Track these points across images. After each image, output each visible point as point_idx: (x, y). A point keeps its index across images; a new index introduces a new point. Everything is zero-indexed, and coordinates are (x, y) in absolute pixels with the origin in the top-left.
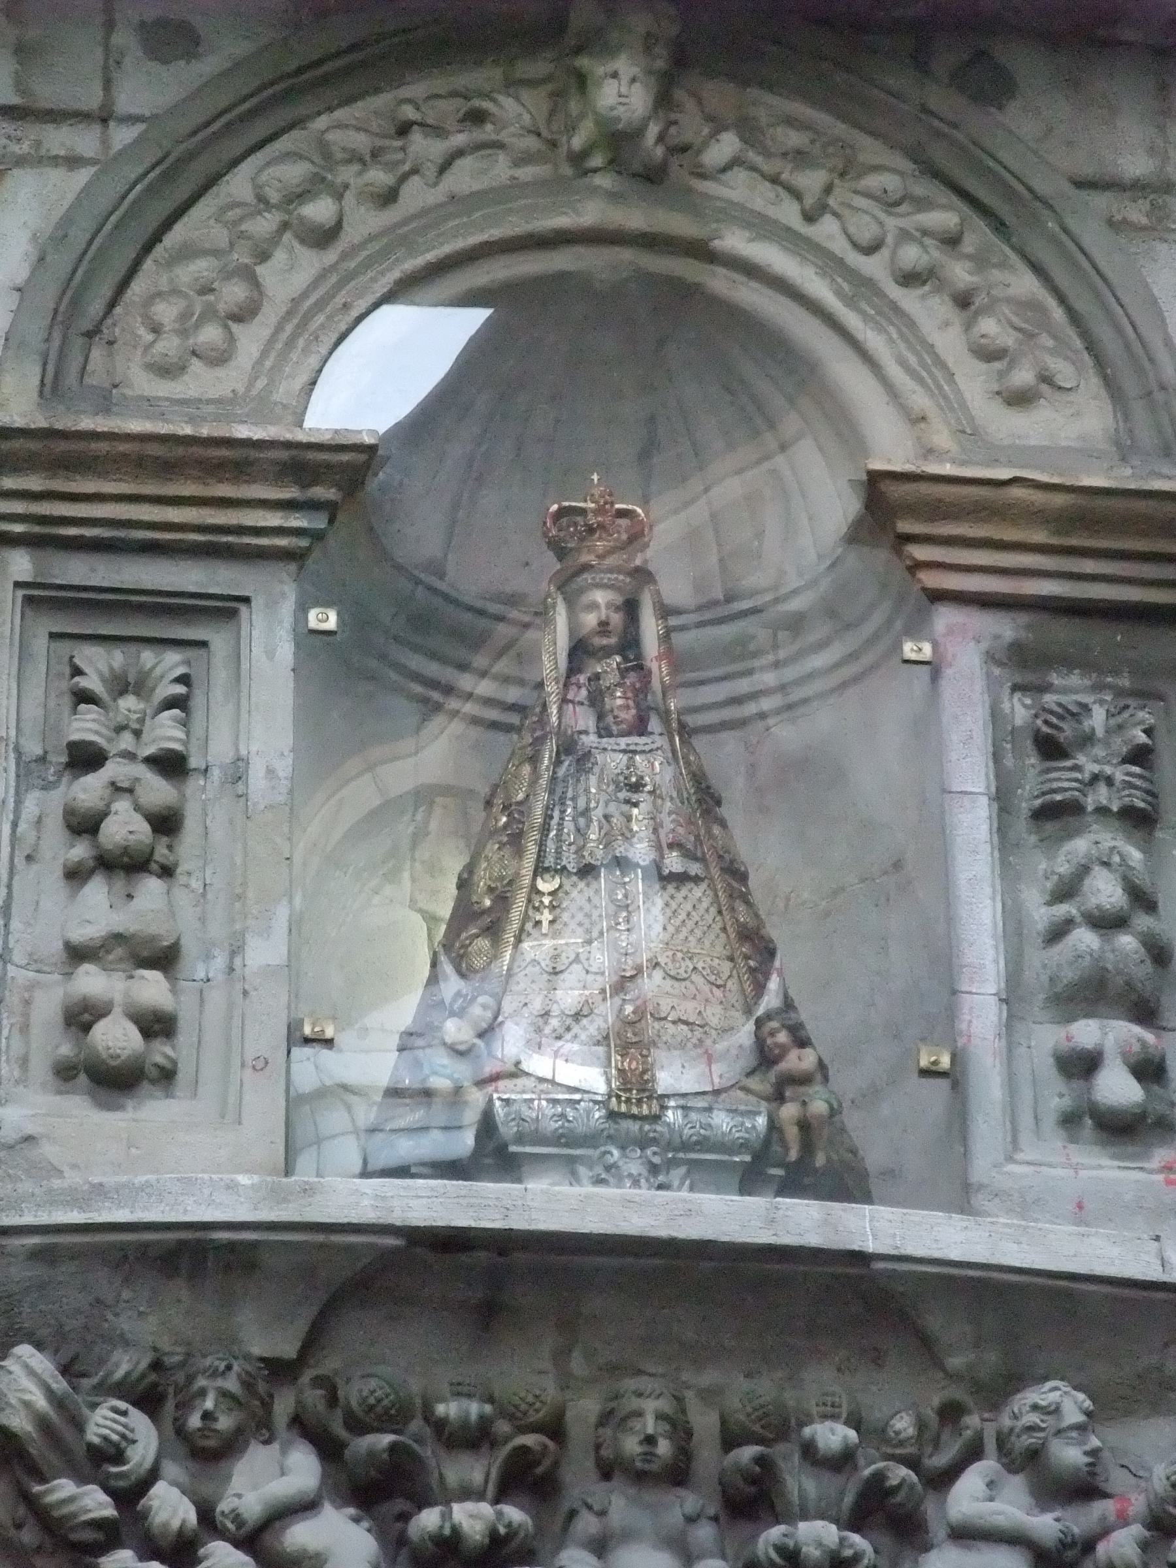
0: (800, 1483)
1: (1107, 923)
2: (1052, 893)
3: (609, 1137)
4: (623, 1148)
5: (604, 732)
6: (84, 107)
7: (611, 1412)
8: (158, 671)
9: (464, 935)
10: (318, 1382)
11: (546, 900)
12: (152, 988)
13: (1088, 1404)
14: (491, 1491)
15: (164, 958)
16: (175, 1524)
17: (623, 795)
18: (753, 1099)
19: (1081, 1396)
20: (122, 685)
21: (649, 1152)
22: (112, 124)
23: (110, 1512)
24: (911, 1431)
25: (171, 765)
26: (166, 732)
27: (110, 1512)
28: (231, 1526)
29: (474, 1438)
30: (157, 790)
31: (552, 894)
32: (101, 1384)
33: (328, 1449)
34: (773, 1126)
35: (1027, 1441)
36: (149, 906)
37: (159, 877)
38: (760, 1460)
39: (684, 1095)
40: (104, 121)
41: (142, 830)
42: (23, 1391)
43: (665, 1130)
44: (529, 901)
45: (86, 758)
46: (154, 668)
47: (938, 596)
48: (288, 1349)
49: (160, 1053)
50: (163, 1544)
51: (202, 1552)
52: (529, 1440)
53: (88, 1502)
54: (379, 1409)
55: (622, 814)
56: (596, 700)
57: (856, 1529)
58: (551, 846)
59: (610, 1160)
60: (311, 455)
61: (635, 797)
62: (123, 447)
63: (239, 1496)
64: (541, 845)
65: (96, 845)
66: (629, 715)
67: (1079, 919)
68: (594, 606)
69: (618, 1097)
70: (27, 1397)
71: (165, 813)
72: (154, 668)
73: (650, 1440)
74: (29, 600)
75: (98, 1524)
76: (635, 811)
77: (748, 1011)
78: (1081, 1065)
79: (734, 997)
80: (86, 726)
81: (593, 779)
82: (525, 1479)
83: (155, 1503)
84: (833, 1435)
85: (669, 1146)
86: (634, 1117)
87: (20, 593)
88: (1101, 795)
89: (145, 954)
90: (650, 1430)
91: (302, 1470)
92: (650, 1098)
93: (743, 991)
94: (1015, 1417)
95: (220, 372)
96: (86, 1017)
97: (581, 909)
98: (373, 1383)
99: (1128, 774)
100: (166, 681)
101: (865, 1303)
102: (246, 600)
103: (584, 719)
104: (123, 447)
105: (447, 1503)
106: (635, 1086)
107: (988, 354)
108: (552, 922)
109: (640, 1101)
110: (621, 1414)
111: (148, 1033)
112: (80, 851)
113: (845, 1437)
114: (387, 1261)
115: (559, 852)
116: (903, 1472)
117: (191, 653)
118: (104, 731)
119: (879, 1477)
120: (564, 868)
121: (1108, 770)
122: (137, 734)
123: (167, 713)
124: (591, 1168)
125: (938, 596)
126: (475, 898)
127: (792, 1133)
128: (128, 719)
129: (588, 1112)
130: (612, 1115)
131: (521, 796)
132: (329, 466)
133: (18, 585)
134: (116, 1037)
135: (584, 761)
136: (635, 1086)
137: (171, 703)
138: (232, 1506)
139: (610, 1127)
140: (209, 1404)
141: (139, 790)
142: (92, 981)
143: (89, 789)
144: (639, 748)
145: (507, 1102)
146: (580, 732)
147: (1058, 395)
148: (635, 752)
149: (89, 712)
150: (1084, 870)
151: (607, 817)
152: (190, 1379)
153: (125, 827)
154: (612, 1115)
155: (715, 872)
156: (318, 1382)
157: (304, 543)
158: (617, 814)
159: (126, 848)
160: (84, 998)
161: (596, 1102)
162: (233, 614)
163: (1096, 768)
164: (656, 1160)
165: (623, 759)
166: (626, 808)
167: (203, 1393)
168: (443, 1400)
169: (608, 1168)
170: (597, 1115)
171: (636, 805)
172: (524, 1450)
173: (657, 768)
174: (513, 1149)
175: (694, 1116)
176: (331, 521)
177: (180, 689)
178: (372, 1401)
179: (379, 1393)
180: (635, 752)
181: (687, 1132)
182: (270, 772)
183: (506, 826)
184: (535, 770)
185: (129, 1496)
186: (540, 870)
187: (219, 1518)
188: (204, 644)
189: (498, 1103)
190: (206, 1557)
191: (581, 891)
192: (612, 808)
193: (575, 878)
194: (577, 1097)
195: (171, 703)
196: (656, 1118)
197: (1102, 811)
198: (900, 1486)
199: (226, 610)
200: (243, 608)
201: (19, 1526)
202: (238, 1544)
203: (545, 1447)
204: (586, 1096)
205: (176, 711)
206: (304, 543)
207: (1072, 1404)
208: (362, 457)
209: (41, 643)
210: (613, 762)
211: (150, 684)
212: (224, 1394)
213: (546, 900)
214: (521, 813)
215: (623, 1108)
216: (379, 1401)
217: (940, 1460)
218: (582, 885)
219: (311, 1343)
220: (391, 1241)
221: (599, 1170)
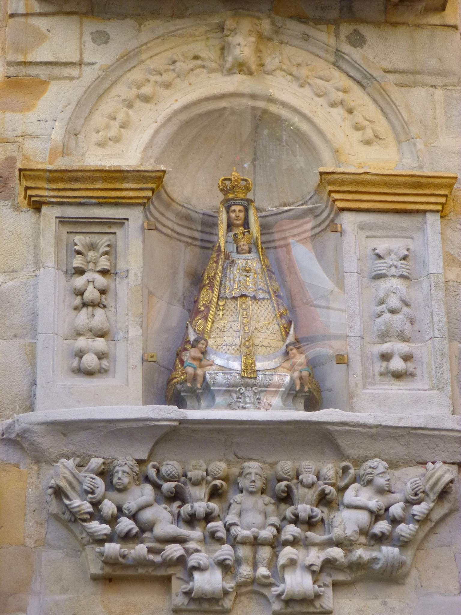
0: (299, 492)
1: (393, 311)
2: (378, 303)
3: (242, 384)
4: (246, 387)
5: (238, 252)
6: (74, 61)
7: (242, 472)
8: (100, 244)
9: (196, 319)
10: (154, 467)
11: (221, 308)
12: (100, 344)
13: (387, 465)
14: (207, 498)
15: (102, 334)
16: (110, 513)
17: (244, 273)
18: (285, 370)
19: (384, 463)
20: (92, 247)
21: (254, 389)
22: (83, 66)
23: (91, 510)
24: (334, 475)
25: (104, 272)
26: (104, 263)
27: (91, 510)
28: (127, 512)
29: (196, 483)
30: (101, 280)
31: (223, 305)
32: (88, 469)
33: (157, 487)
34: (291, 378)
35: (369, 477)
36: (99, 318)
37: (102, 308)
38: (288, 486)
39: (264, 370)
40: (80, 65)
41: (97, 293)
42: (64, 473)
43: (259, 382)
44: (216, 308)
45: (80, 272)
46: (99, 242)
47: (343, 210)
48: (144, 456)
49: (105, 363)
50: (107, 519)
51: (119, 520)
52: (218, 482)
53: (84, 507)
54: (171, 475)
55: (244, 280)
56: (236, 241)
57: (317, 506)
58: (222, 291)
59: (242, 391)
60: (146, 174)
61: (248, 274)
62: (87, 174)
63: (129, 503)
64: (220, 290)
65: (82, 299)
66: (246, 248)
67: (386, 311)
68: (234, 211)
69: (244, 372)
70: (65, 475)
71: (104, 289)
72: (99, 242)
73: (253, 481)
74: (60, 222)
75: (89, 513)
76: (248, 279)
77: (284, 340)
78: (80, 354)
79: (280, 338)
80: (78, 262)
81: (235, 268)
82: (215, 494)
83: (104, 506)
84: (309, 478)
85: (260, 386)
86: (249, 378)
87: (58, 220)
88: (393, 271)
89: (99, 333)
90: (253, 478)
91: (147, 493)
92: (254, 371)
93: (282, 334)
94: (365, 470)
95: (118, 145)
96: (81, 354)
97: (232, 310)
98: (169, 467)
99: (402, 264)
100: (103, 246)
101: (323, 438)
102: (127, 219)
103: (232, 247)
104: (87, 174)
105: (192, 502)
106: (249, 369)
107: (358, 128)
108: (223, 315)
109: (251, 373)
110: (245, 473)
111: (100, 358)
112: (78, 301)
113: (313, 479)
114: (174, 429)
115: (225, 292)
116: (331, 488)
117: (111, 236)
118: (83, 262)
119: (323, 490)
120: (226, 297)
121: (395, 263)
122: (95, 263)
123: (103, 257)
124: (236, 394)
125: (343, 210)
126: (199, 307)
127: (298, 382)
128: (91, 259)
129: (235, 377)
130: (242, 377)
131: (213, 274)
132: (151, 177)
133: (56, 218)
134: (90, 360)
135: (232, 263)
136: (249, 369)
137: (106, 253)
138: (127, 506)
139: (242, 381)
140: (120, 475)
141: (95, 281)
142: (82, 342)
143: (79, 282)
144: (250, 258)
145: (211, 374)
146: (231, 252)
147: (380, 141)
148: (248, 259)
149: (79, 257)
150: (387, 295)
151: (239, 281)
152: (114, 467)
153: (91, 294)
154: (242, 377)
155: (273, 297)
156: (154, 467)
157: (145, 201)
158: (242, 280)
159: (92, 300)
160: (80, 348)
161: (237, 373)
162: (123, 224)
163: (391, 263)
164: (256, 391)
165: (244, 262)
166: (245, 278)
167: (118, 472)
168: (191, 471)
169: (241, 394)
170: (238, 377)
171: (248, 277)
172: (216, 485)
173: (254, 264)
174: (212, 388)
175: (267, 377)
176: (153, 193)
177: (107, 249)
178: (169, 472)
179: (171, 470)
180: (248, 259)
181: (265, 382)
182: (136, 274)
183: (208, 284)
184: (217, 266)
185: (96, 504)
186: (219, 298)
187: (124, 510)
188: (115, 233)
189: (207, 374)
190: (120, 522)
191: (232, 305)
192: (241, 278)
193: (229, 301)
194: (231, 372)
195: (106, 253)
196: (255, 378)
197: (394, 276)
198: (330, 492)
199: (121, 222)
200: (126, 222)
201: (64, 514)
202: (129, 518)
203: (222, 485)
204: (235, 372)
205: (106, 256)
206: (145, 201)
207: (380, 465)
208: (162, 174)
209: (64, 235)
210: (240, 262)
211: (98, 247)
212: (124, 472)
213: (221, 308)
214: (213, 280)
215: (246, 375)
216: (171, 472)
217: (342, 484)
218: (232, 303)
219: (151, 453)
220: (176, 423)
221: (238, 394)
